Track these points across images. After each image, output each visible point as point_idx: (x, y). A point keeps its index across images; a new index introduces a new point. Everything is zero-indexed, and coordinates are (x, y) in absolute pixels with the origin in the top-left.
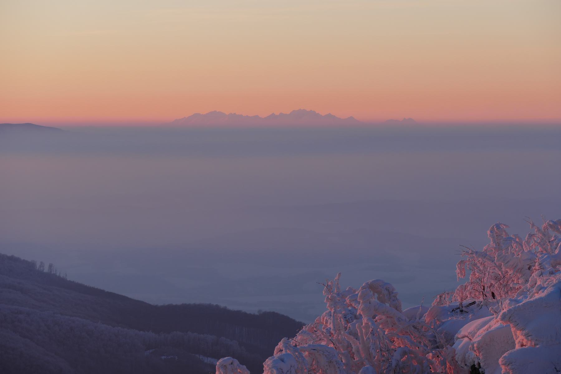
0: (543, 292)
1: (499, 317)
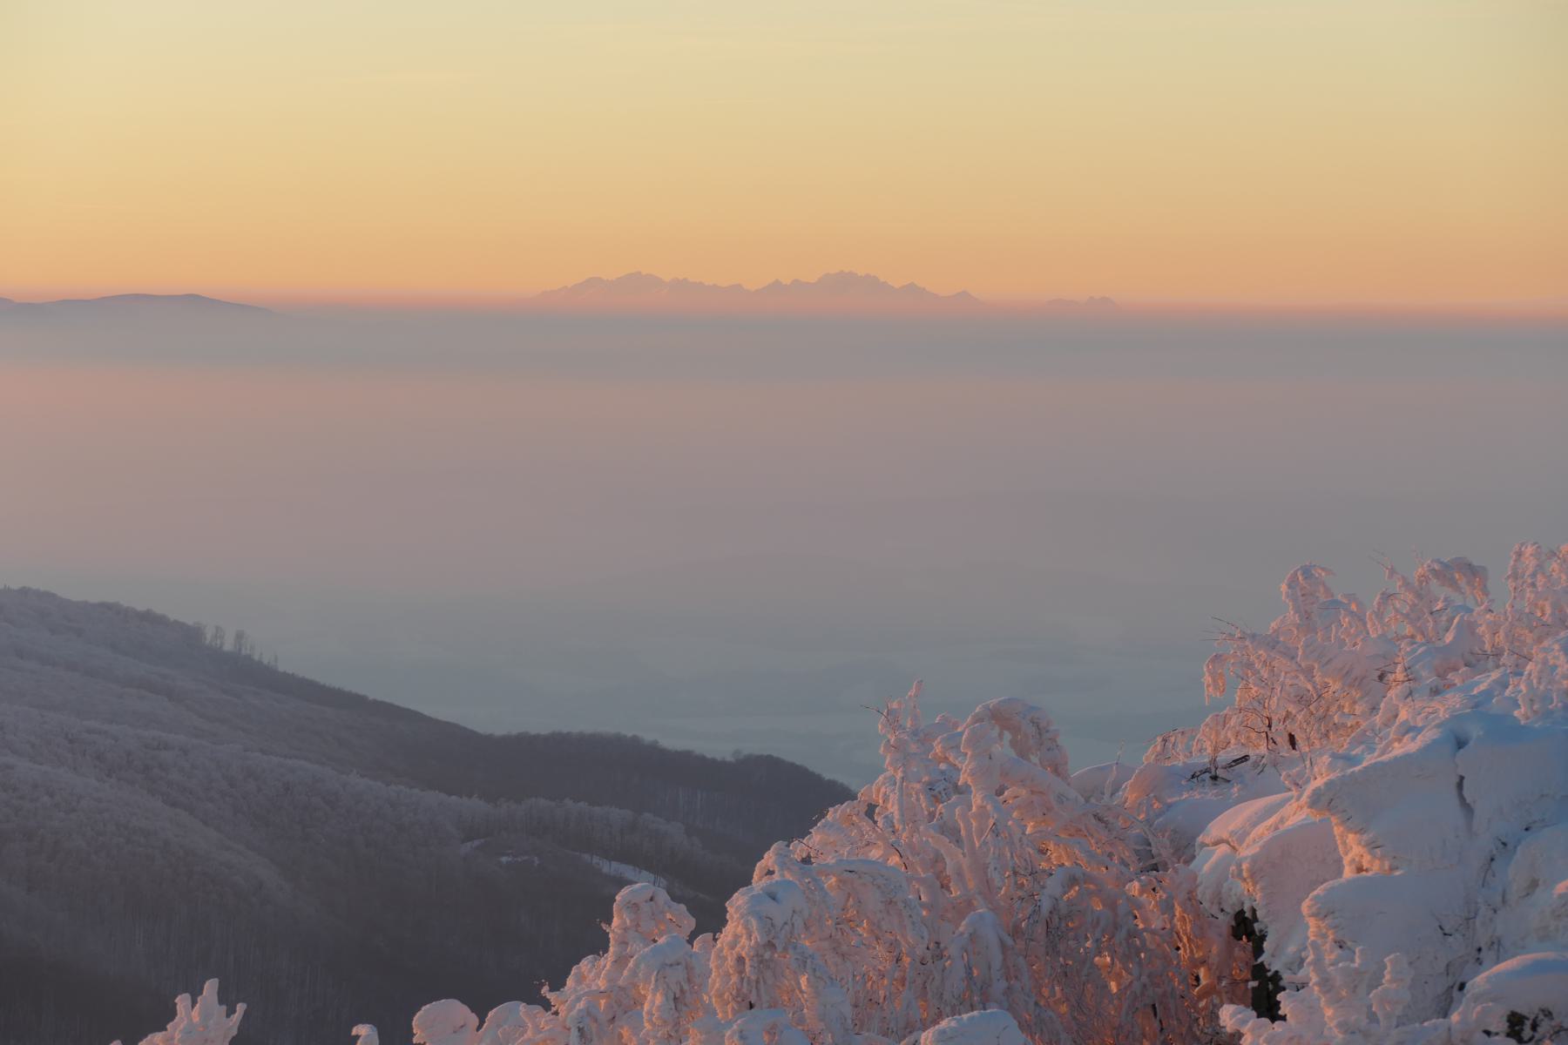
0: (1413, 739)
1: (1305, 798)
